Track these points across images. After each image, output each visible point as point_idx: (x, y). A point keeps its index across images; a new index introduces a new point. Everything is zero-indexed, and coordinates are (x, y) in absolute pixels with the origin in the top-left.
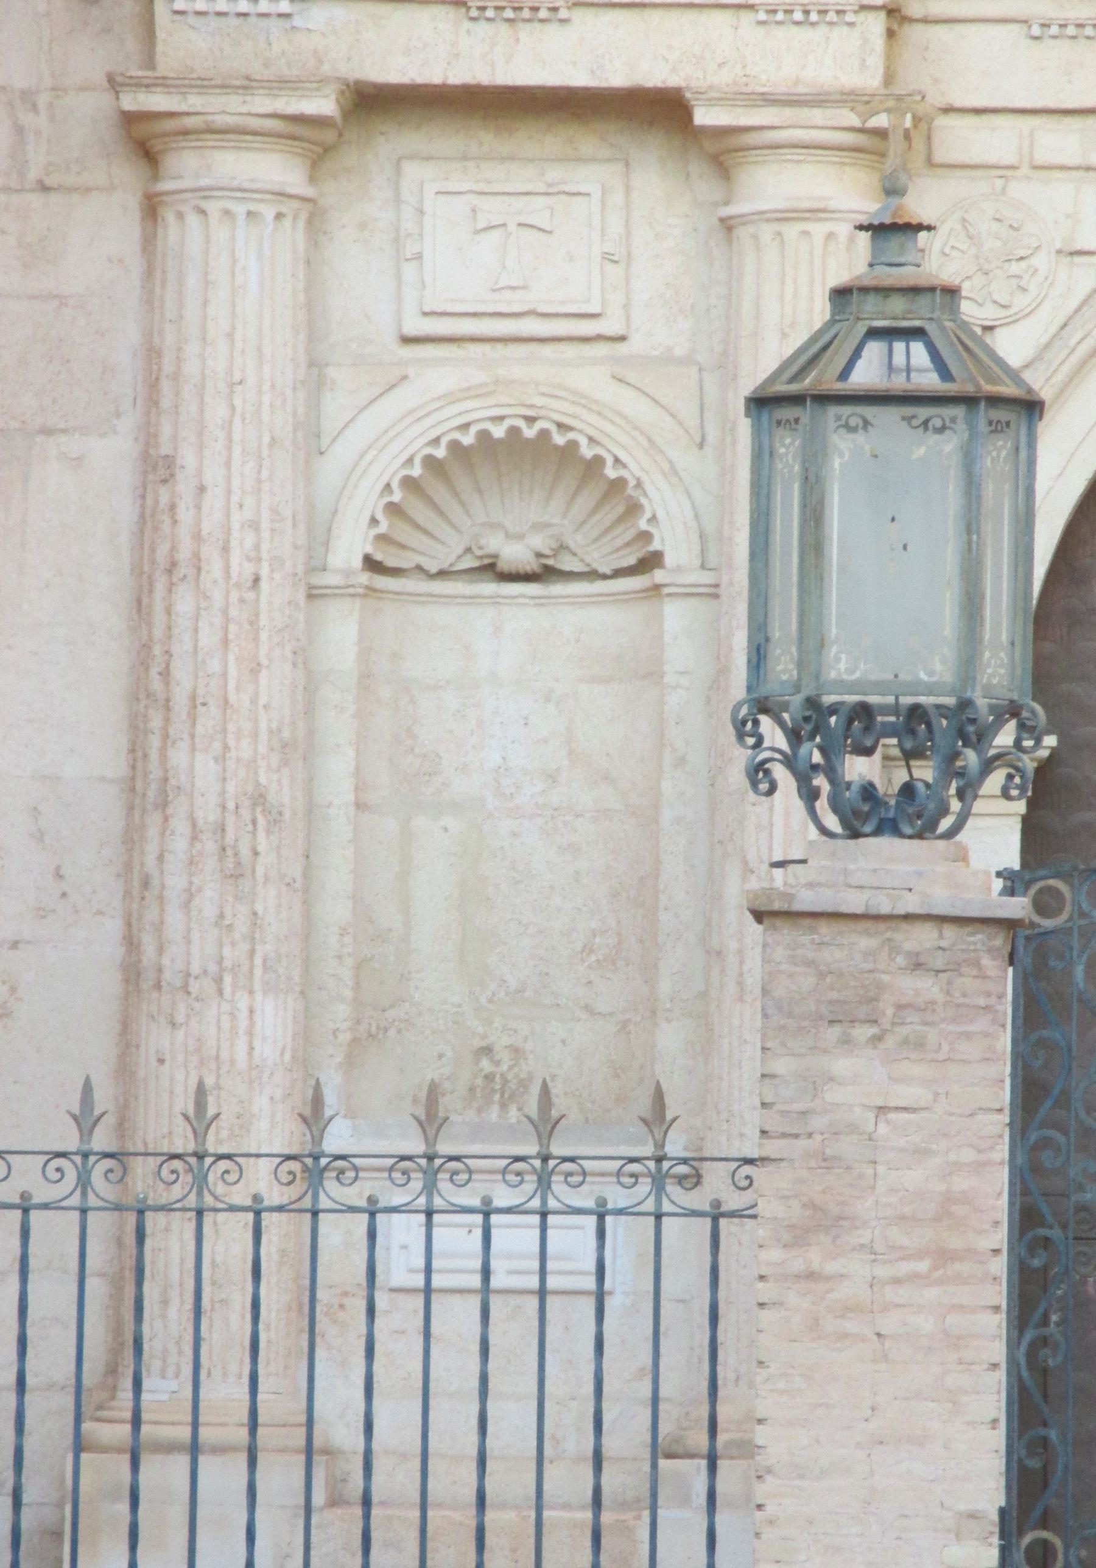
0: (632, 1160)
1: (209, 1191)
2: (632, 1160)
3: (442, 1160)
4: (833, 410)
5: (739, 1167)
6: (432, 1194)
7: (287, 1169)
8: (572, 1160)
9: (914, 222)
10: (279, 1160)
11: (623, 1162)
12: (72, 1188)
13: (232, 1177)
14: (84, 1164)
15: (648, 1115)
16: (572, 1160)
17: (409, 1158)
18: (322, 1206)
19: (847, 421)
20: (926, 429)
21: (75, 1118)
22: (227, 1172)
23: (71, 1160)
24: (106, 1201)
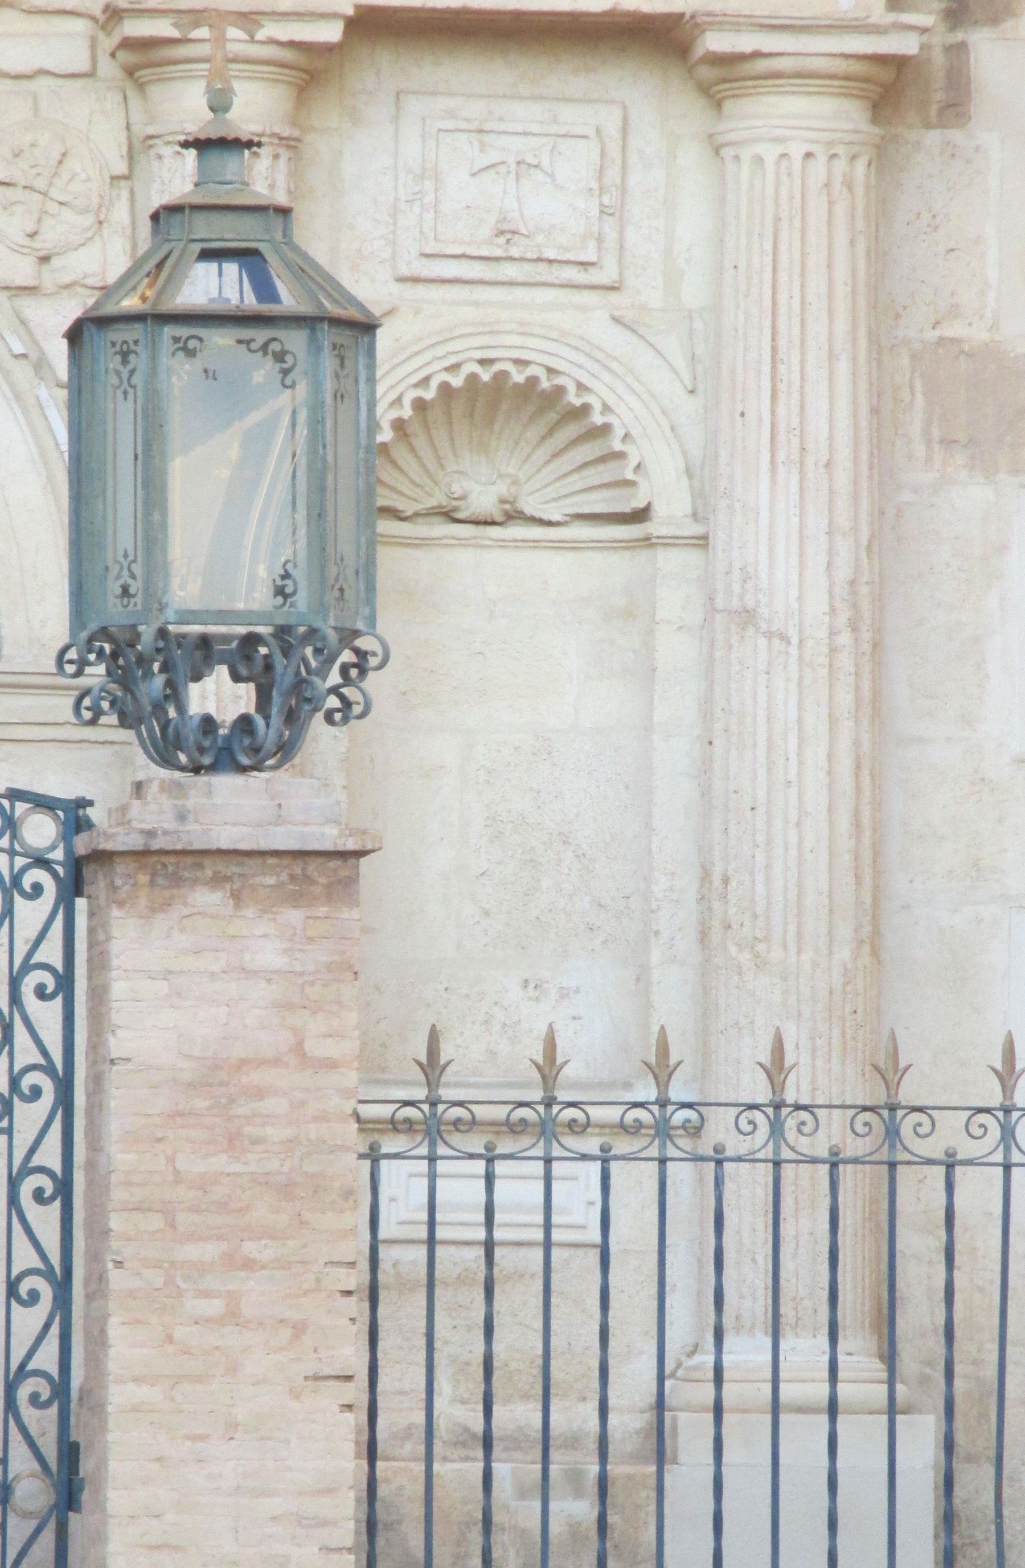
0: (521, 1104)
1: (788, 1145)
2: (521, 1104)
3: (445, 1106)
4: (169, 331)
5: (857, 1114)
6: (551, 1143)
7: (867, 1119)
8: (460, 1104)
9: (231, 136)
10: (971, 1112)
11: (398, 1105)
12: (881, 1141)
13: (926, 1128)
14: (777, 1115)
15: (767, 1063)
16: (460, 1104)
17: (987, 1110)
18: (669, 1155)
19: (186, 343)
20: (265, 353)
21: (539, 1068)
22: (803, 1123)
23: (994, 1116)
24: (687, 1153)
